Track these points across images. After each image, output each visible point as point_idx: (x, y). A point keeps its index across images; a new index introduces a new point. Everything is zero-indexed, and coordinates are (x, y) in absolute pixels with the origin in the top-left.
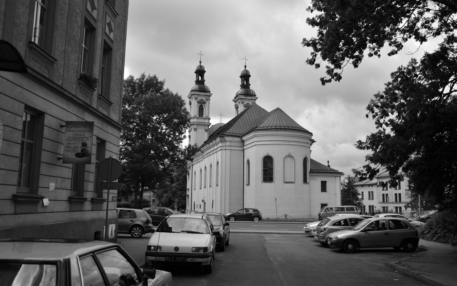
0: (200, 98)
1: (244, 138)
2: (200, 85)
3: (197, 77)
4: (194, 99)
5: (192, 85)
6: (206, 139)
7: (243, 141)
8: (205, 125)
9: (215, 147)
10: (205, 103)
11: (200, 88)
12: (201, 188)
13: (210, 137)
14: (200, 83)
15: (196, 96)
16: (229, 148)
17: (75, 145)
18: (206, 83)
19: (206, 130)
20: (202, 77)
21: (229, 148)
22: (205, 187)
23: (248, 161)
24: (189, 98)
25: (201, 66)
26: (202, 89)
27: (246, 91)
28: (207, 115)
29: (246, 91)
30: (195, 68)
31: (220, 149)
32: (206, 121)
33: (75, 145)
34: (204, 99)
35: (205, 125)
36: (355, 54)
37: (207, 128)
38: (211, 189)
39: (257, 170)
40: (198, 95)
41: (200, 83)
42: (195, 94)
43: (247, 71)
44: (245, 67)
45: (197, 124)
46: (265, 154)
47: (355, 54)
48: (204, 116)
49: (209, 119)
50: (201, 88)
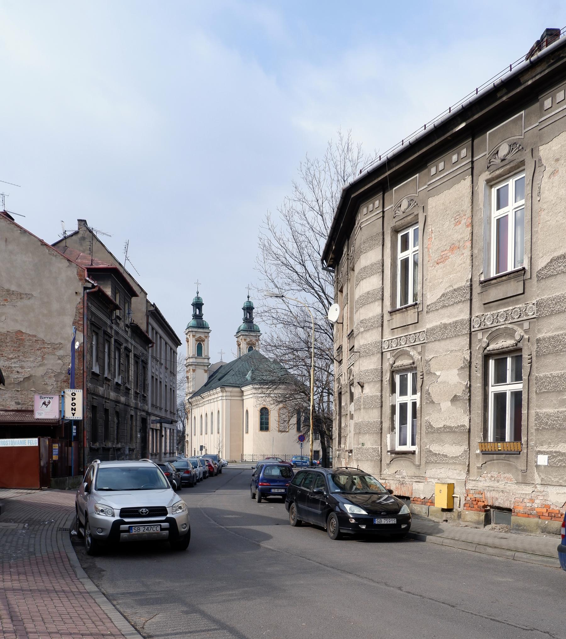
0: (198, 335)
1: (243, 389)
2: (199, 320)
3: (195, 311)
4: (191, 336)
5: (189, 319)
6: (205, 381)
7: (242, 392)
8: (204, 366)
9: (216, 396)
10: (203, 341)
11: (198, 323)
12: (201, 434)
13: (209, 378)
14: (198, 317)
15: (194, 333)
16: (230, 398)
17: (496, 484)
18: (204, 318)
19: (206, 371)
20: (200, 310)
21: (230, 398)
22: (206, 434)
23: (247, 411)
24: (186, 334)
25: (198, 298)
26: (201, 325)
27: (249, 326)
28: (206, 354)
29: (249, 326)
30: (191, 299)
31: (220, 398)
32: (206, 361)
33: (496, 484)
34: (203, 336)
35: (204, 366)
36: (76, 533)
37: (206, 368)
38: (212, 436)
39: (254, 420)
40: (196, 332)
41: (198, 317)
42: (192, 331)
43: (250, 302)
44: (248, 297)
45: (195, 365)
46: (262, 406)
47: (76, 533)
48: (203, 356)
49: (208, 359)
50: (199, 323)
